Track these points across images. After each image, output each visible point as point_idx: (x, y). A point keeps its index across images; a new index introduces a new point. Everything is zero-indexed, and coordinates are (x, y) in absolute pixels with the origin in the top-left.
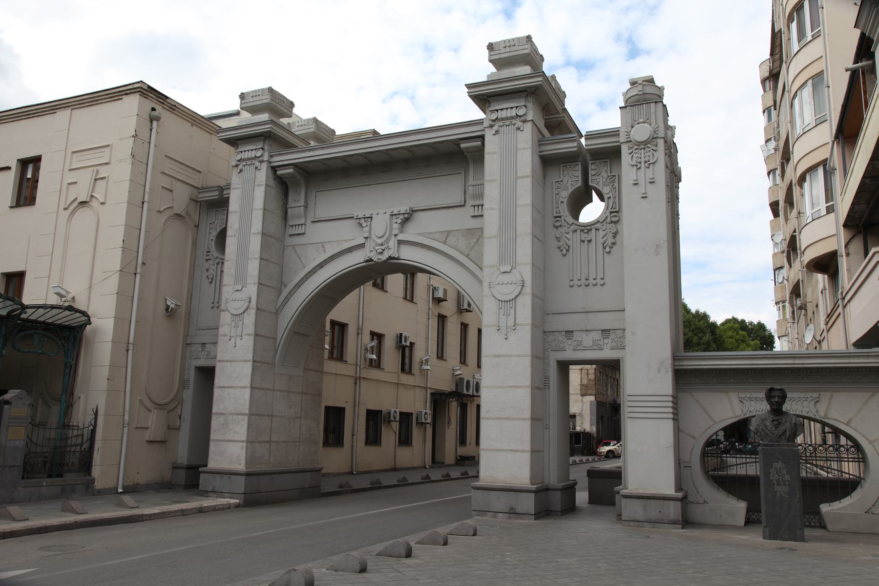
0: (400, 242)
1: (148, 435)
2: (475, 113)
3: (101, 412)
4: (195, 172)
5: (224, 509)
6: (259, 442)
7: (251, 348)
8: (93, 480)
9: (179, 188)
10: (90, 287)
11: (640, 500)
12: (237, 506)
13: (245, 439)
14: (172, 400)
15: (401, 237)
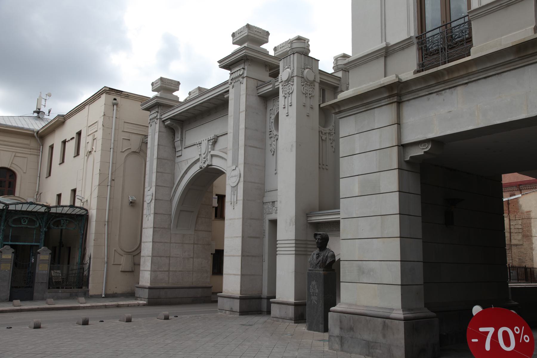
0: (212, 156)
1: (121, 268)
2: (225, 75)
3: (92, 257)
4: (145, 127)
5: (131, 306)
6: (161, 271)
7: (153, 221)
8: (88, 291)
9: (133, 137)
11: (278, 305)
12: (144, 305)
13: (150, 269)
14: (137, 249)
15: (213, 153)
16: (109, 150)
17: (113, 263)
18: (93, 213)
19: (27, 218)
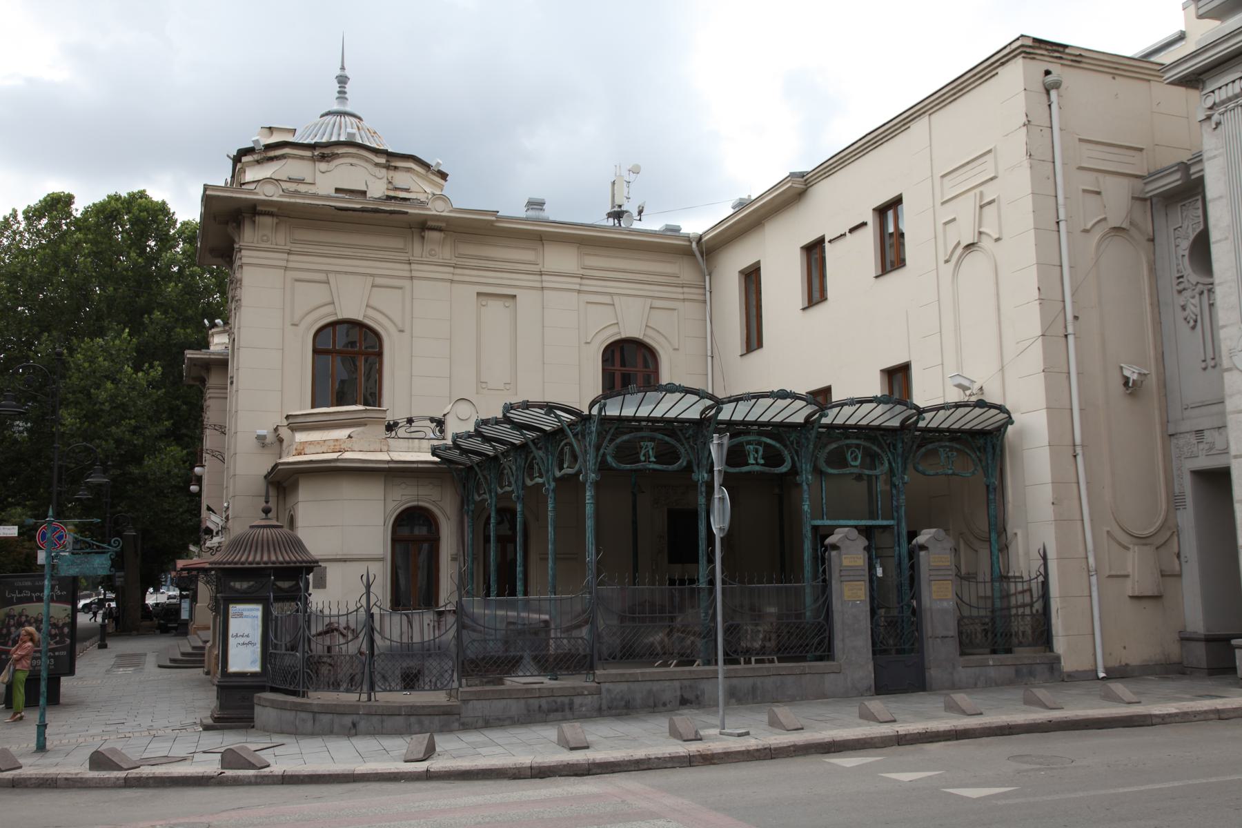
1: (1130, 588)
3: (1051, 555)
10: (1002, 369)
16: (1054, 227)
17: (1107, 574)
18: (1032, 420)
19: (858, 446)
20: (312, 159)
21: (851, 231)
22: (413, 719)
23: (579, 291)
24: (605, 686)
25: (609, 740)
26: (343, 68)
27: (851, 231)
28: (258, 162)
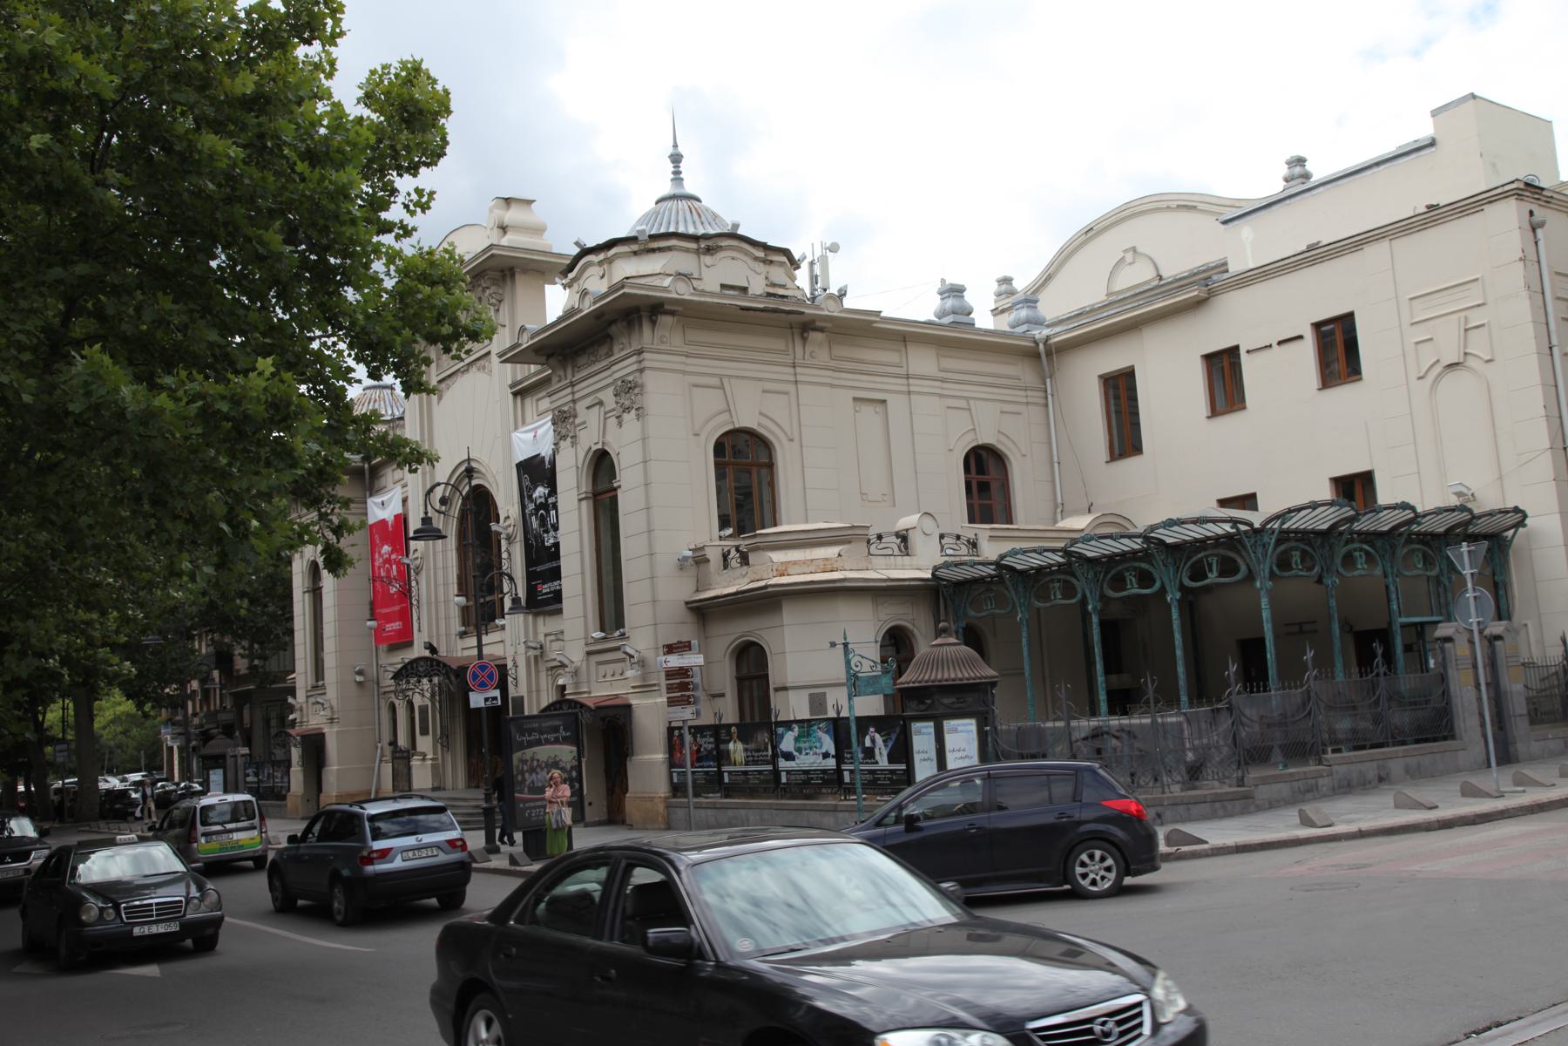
10: (1501, 478)
20: (697, 252)
21: (1280, 343)
22: (1217, 805)
23: (941, 396)
24: (1335, 768)
25: (1351, 814)
26: (675, 146)
27: (1280, 343)
28: (635, 253)
